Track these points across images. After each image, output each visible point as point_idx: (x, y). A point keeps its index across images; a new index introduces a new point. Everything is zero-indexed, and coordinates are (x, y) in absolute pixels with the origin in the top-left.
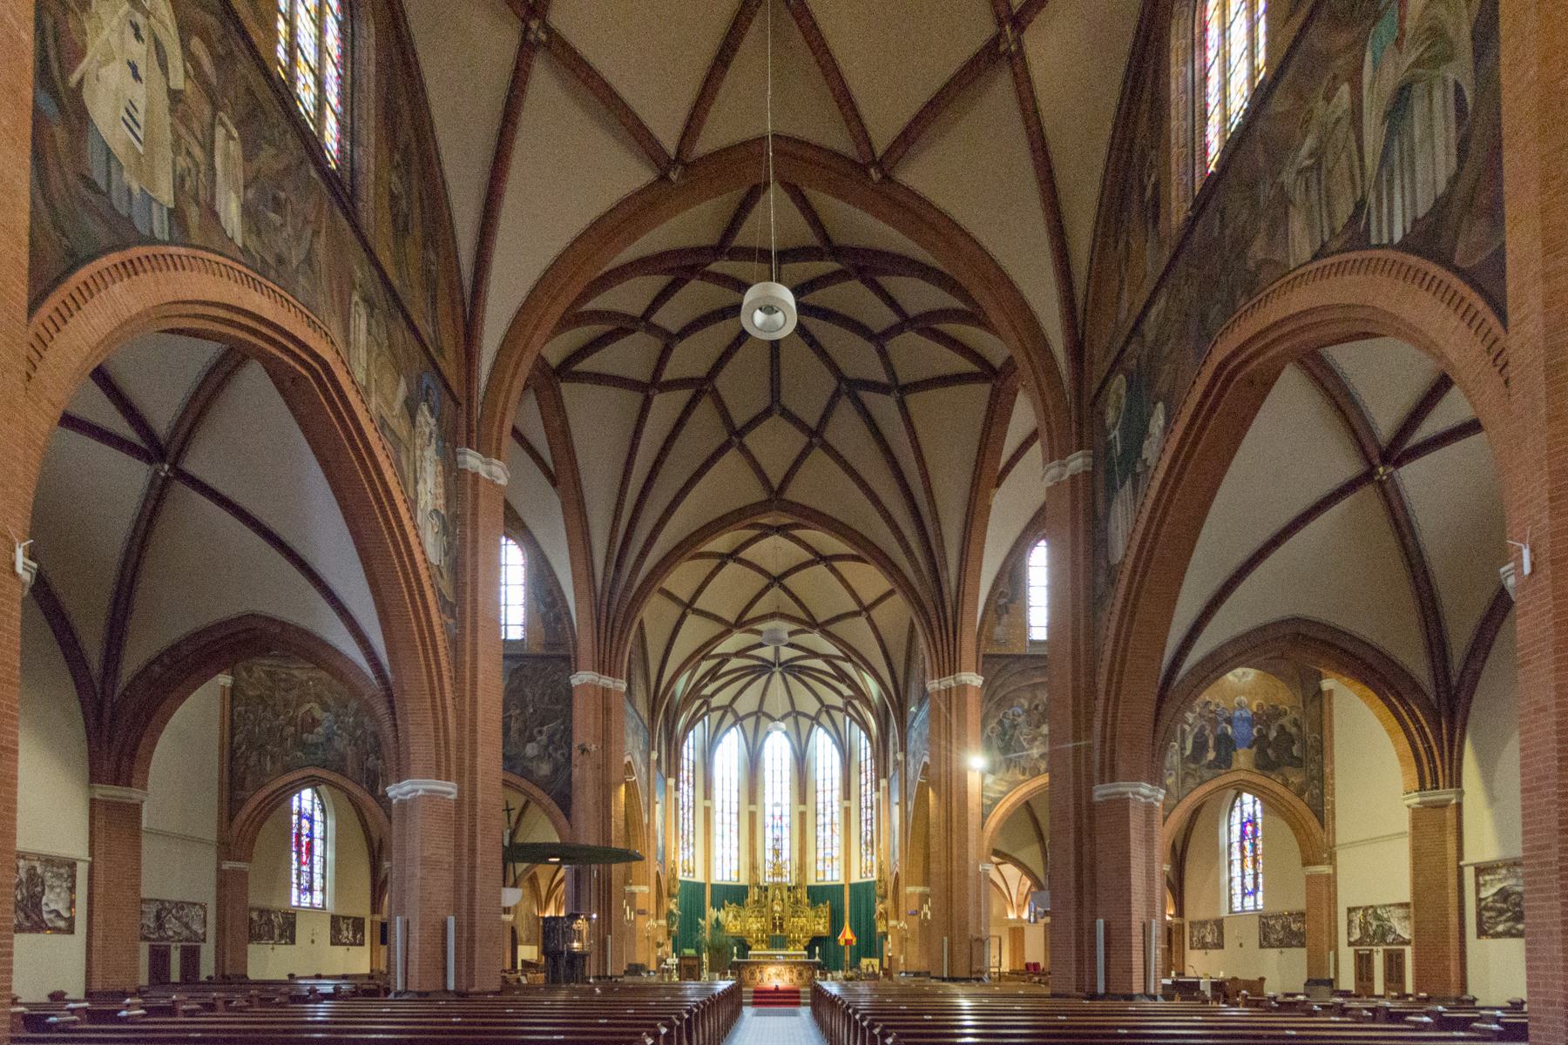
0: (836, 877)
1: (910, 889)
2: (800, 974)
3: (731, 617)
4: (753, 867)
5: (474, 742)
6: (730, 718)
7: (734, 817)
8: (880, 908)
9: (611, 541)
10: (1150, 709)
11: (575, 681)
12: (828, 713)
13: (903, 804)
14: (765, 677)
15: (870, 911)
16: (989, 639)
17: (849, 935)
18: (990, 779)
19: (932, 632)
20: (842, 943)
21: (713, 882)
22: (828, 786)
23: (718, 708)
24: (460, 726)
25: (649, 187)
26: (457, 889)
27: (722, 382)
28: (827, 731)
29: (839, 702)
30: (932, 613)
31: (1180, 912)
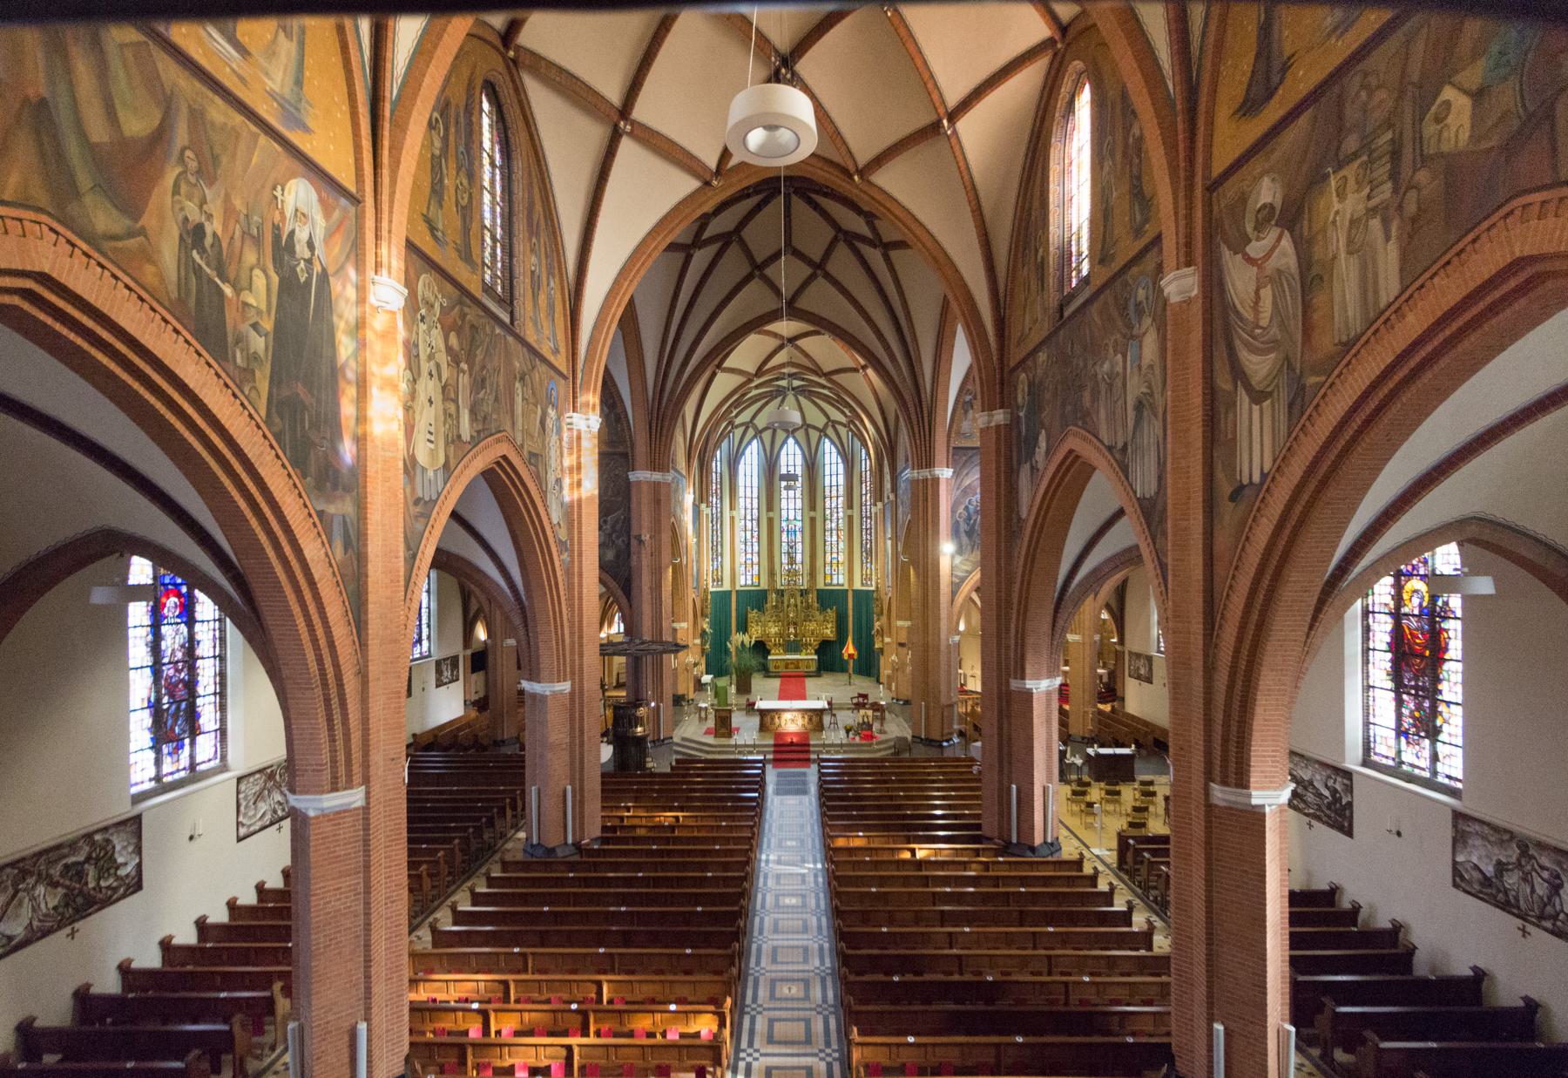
0: (841, 581)
1: (900, 623)
2: (810, 719)
3: (752, 369)
4: (772, 573)
5: (581, 645)
6: (751, 432)
7: (755, 523)
8: (877, 625)
9: (658, 367)
10: (1049, 619)
11: (634, 476)
12: (834, 427)
13: (895, 538)
14: (780, 399)
15: (870, 627)
16: (959, 433)
17: (851, 650)
18: (958, 560)
19: (911, 423)
20: (846, 657)
21: (738, 588)
22: (834, 493)
23: (742, 425)
24: (572, 634)
25: (697, 191)
26: (572, 763)
27: (746, 233)
28: (832, 442)
29: (844, 420)
30: (912, 410)
31: (1122, 641)
